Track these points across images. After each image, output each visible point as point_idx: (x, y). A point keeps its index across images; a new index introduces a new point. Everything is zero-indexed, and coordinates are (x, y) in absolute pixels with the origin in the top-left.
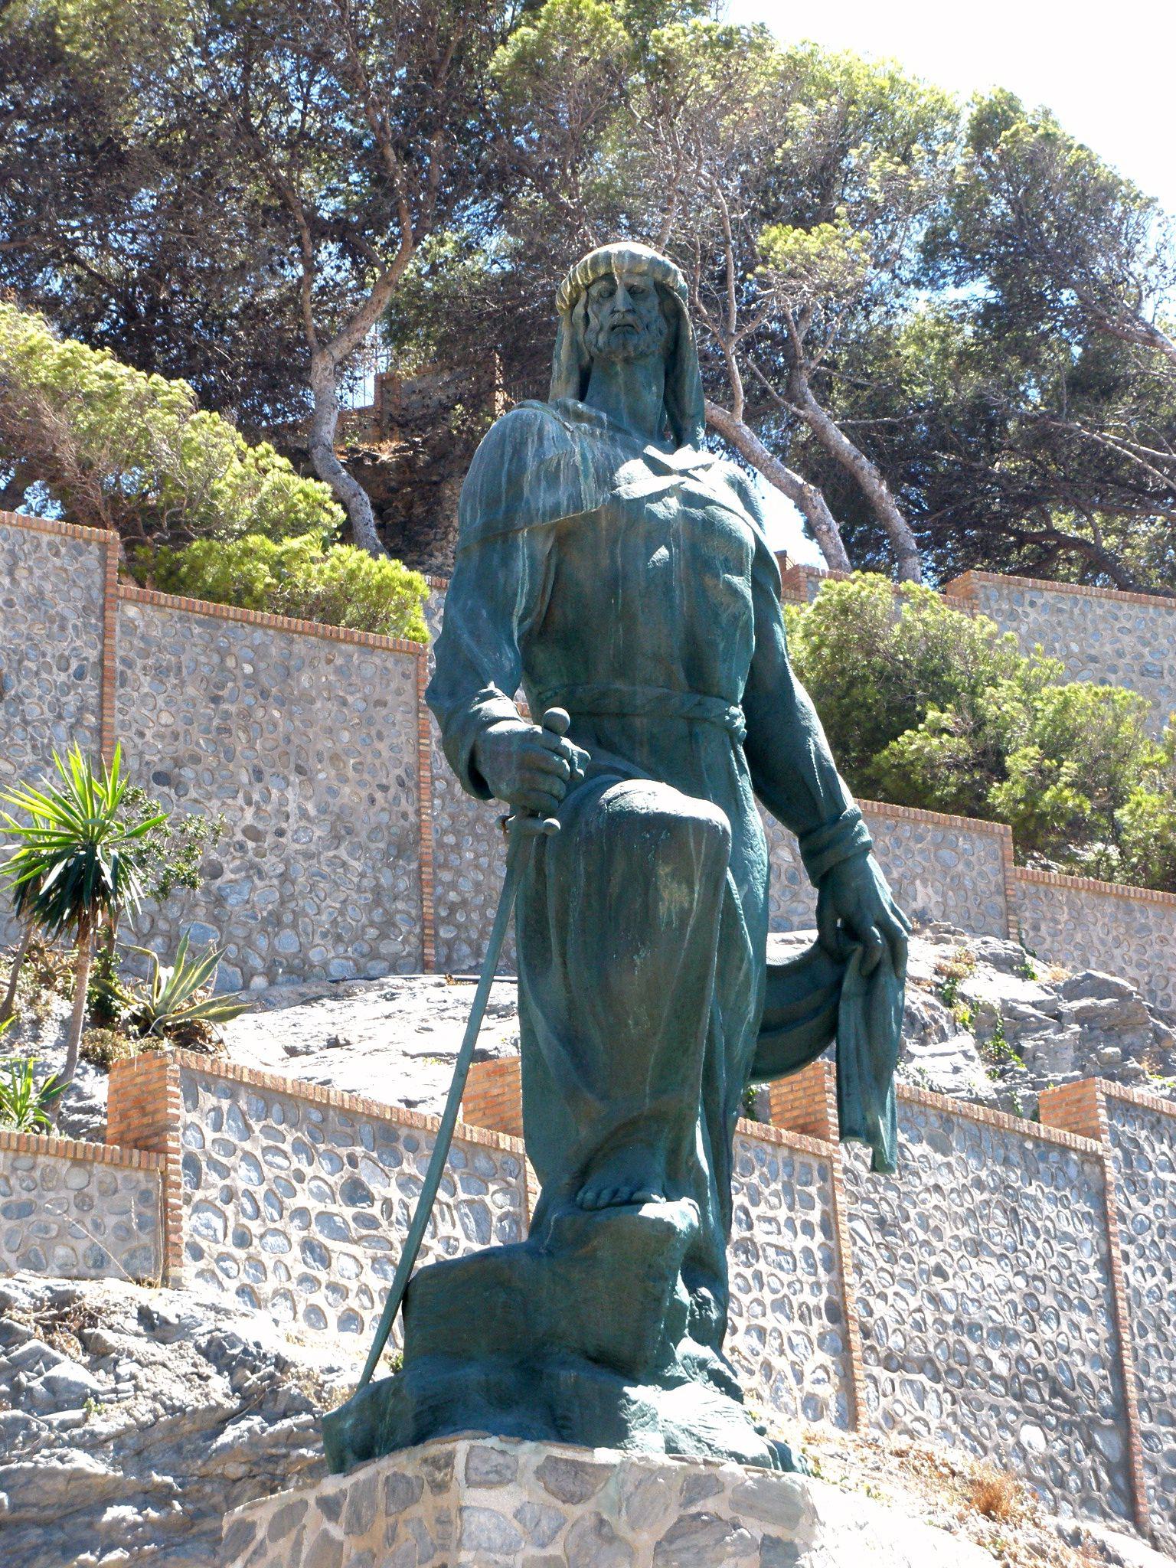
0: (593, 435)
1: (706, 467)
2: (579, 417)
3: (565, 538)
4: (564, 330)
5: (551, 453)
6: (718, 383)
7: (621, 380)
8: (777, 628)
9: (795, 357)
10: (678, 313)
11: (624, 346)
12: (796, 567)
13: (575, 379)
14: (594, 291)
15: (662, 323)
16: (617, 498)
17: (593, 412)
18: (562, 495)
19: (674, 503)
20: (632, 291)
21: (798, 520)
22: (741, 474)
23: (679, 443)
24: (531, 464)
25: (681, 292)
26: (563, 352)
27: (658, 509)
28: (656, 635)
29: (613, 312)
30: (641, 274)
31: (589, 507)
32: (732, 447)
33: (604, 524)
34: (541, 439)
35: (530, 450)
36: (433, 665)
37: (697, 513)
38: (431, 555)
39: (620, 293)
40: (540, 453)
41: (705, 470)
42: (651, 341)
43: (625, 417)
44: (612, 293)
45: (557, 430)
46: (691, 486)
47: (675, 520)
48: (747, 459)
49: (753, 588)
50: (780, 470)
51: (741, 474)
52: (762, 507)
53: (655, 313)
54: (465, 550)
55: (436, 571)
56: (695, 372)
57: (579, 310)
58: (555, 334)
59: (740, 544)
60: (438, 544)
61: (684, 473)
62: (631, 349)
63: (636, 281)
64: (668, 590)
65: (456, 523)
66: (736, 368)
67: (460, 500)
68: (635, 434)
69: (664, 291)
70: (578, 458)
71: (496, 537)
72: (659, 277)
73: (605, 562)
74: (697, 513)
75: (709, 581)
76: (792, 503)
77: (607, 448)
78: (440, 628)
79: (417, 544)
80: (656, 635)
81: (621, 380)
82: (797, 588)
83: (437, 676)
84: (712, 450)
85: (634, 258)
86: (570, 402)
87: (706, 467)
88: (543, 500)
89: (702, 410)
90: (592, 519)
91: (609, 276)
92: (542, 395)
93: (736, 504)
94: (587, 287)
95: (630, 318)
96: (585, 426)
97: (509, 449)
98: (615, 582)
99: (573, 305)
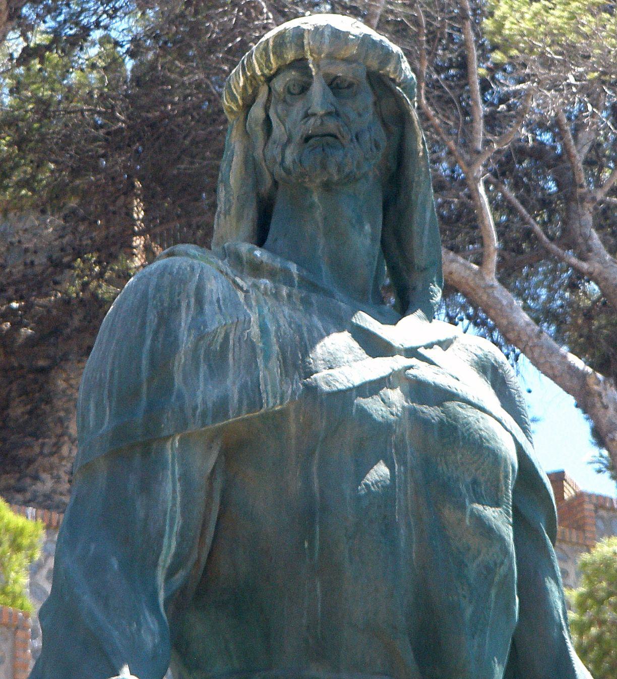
0: (276, 296)
1: (445, 345)
2: (256, 269)
3: (235, 450)
4: (235, 142)
5: (215, 323)
6: (461, 224)
7: (318, 214)
8: (551, 585)
9: (574, 184)
10: (403, 118)
11: (324, 167)
12: (580, 497)
13: (251, 213)
14: (279, 85)
15: (379, 133)
16: (312, 390)
17: (278, 263)
18: (232, 385)
19: (396, 396)
20: (335, 85)
21: (582, 426)
22: (497, 355)
23: (403, 309)
24: (186, 340)
25: (407, 86)
26: (233, 173)
27: (373, 405)
28: (372, 597)
29: (307, 116)
30: (347, 61)
31: (271, 404)
32: (484, 318)
33: (293, 428)
34: (200, 302)
35: (185, 319)
36: (38, 643)
37: (432, 412)
38: (36, 478)
39: (317, 88)
40: (198, 325)
41: (444, 349)
42: (364, 159)
43: (325, 268)
44: (305, 88)
45: (221, 288)
46: (422, 371)
47: (399, 422)
48: (509, 338)
49: (516, 526)
50: (553, 352)
51: (497, 355)
52: (531, 405)
53: (369, 116)
54: (87, 468)
55: (45, 503)
56: (427, 204)
57: (257, 112)
58: (219, 153)
59: (496, 458)
60: (46, 461)
61: (412, 353)
62: (333, 170)
63: (340, 70)
64: (388, 529)
65: (73, 429)
66: (485, 199)
67: (80, 395)
68: (339, 294)
69: (381, 84)
70: (255, 330)
71: (134, 446)
72: (374, 64)
73: (295, 485)
74: (432, 412)
75: (449, 514)
76: (571, 400)
77: (298, 316)
78: (48, 587)
79: (15, 461)
80: (372, 597)
81: (318, 214)
82: (580, 527)
83: (44, 657)
84: (452, 320)
85: (337, 35)
86: (244, 248)
87: (445, 345)
88: (204, 392)
89: (437, 263)
90: (276, 421)
91: (300, 64)
92: (204, 238)
93: (491, 401)
94: (269, 79)
95: (332, 125)
96: (265, 283)
97: (152, 318)
98: (310, 515)
99: (247, 106)
